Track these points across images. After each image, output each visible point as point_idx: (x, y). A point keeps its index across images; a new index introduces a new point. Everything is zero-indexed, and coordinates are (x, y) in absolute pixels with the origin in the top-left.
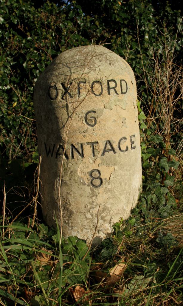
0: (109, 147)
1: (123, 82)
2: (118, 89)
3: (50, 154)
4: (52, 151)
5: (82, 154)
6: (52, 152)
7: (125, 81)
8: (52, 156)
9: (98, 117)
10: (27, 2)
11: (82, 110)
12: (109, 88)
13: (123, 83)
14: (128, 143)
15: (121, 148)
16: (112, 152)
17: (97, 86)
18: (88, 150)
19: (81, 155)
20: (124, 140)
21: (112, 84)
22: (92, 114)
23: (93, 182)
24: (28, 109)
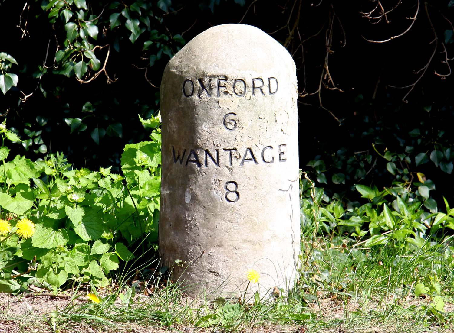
0: (249, 156)
1: (271, 80)
2: (265, 89)
3: (179, 161)
4: (181, 156)
5: (216, 160)
6: (181, 158)
7: (274, 78)
8: (181, 162)
9: (238, 120)
10: (22, 329)
11: (216, 113)
12: (254, 87)
13: (273, 82)
14: (275, 152)
15: (265, 160)
16: (252, 162)
17: (240, 85)
18: (225, 156)
19: (216, 164)
20: (269, 149)
21: (258, 84)
22: (232, 117)
23: (228, 197)
24: (365, 171)
